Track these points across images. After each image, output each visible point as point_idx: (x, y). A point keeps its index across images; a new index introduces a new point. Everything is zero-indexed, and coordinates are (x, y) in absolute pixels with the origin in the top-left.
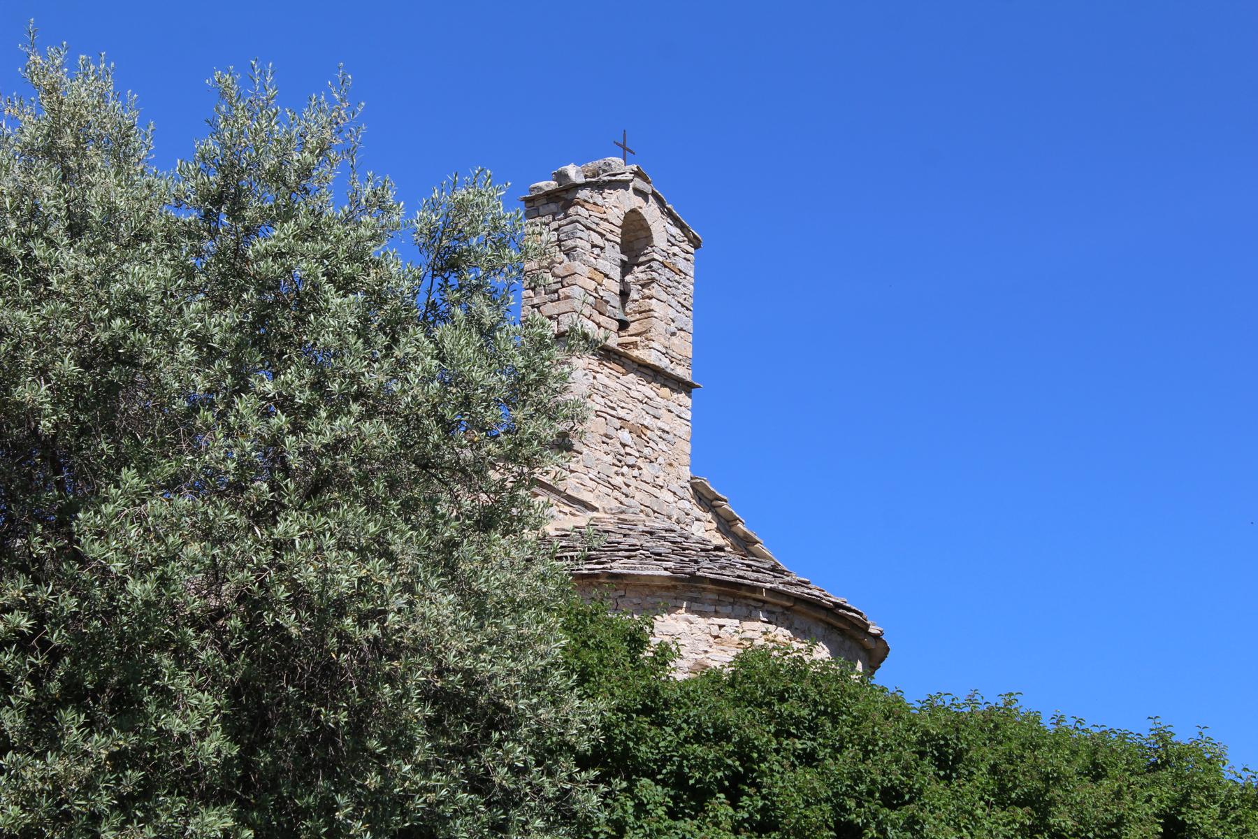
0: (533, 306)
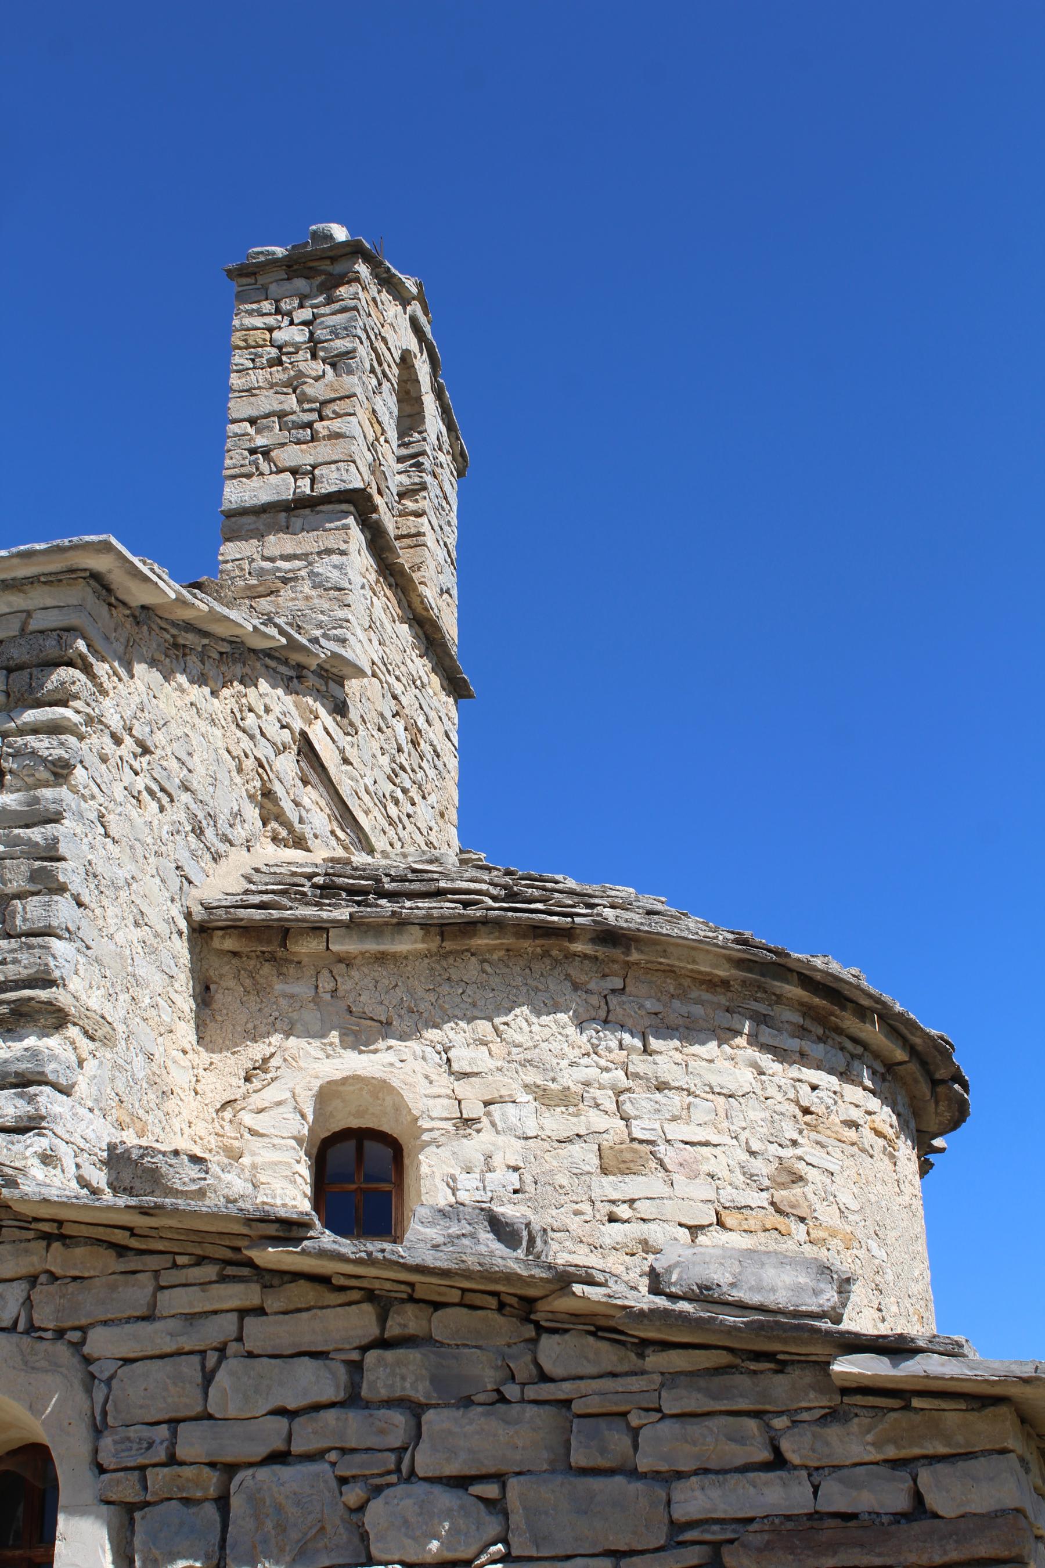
0: (253, 451)
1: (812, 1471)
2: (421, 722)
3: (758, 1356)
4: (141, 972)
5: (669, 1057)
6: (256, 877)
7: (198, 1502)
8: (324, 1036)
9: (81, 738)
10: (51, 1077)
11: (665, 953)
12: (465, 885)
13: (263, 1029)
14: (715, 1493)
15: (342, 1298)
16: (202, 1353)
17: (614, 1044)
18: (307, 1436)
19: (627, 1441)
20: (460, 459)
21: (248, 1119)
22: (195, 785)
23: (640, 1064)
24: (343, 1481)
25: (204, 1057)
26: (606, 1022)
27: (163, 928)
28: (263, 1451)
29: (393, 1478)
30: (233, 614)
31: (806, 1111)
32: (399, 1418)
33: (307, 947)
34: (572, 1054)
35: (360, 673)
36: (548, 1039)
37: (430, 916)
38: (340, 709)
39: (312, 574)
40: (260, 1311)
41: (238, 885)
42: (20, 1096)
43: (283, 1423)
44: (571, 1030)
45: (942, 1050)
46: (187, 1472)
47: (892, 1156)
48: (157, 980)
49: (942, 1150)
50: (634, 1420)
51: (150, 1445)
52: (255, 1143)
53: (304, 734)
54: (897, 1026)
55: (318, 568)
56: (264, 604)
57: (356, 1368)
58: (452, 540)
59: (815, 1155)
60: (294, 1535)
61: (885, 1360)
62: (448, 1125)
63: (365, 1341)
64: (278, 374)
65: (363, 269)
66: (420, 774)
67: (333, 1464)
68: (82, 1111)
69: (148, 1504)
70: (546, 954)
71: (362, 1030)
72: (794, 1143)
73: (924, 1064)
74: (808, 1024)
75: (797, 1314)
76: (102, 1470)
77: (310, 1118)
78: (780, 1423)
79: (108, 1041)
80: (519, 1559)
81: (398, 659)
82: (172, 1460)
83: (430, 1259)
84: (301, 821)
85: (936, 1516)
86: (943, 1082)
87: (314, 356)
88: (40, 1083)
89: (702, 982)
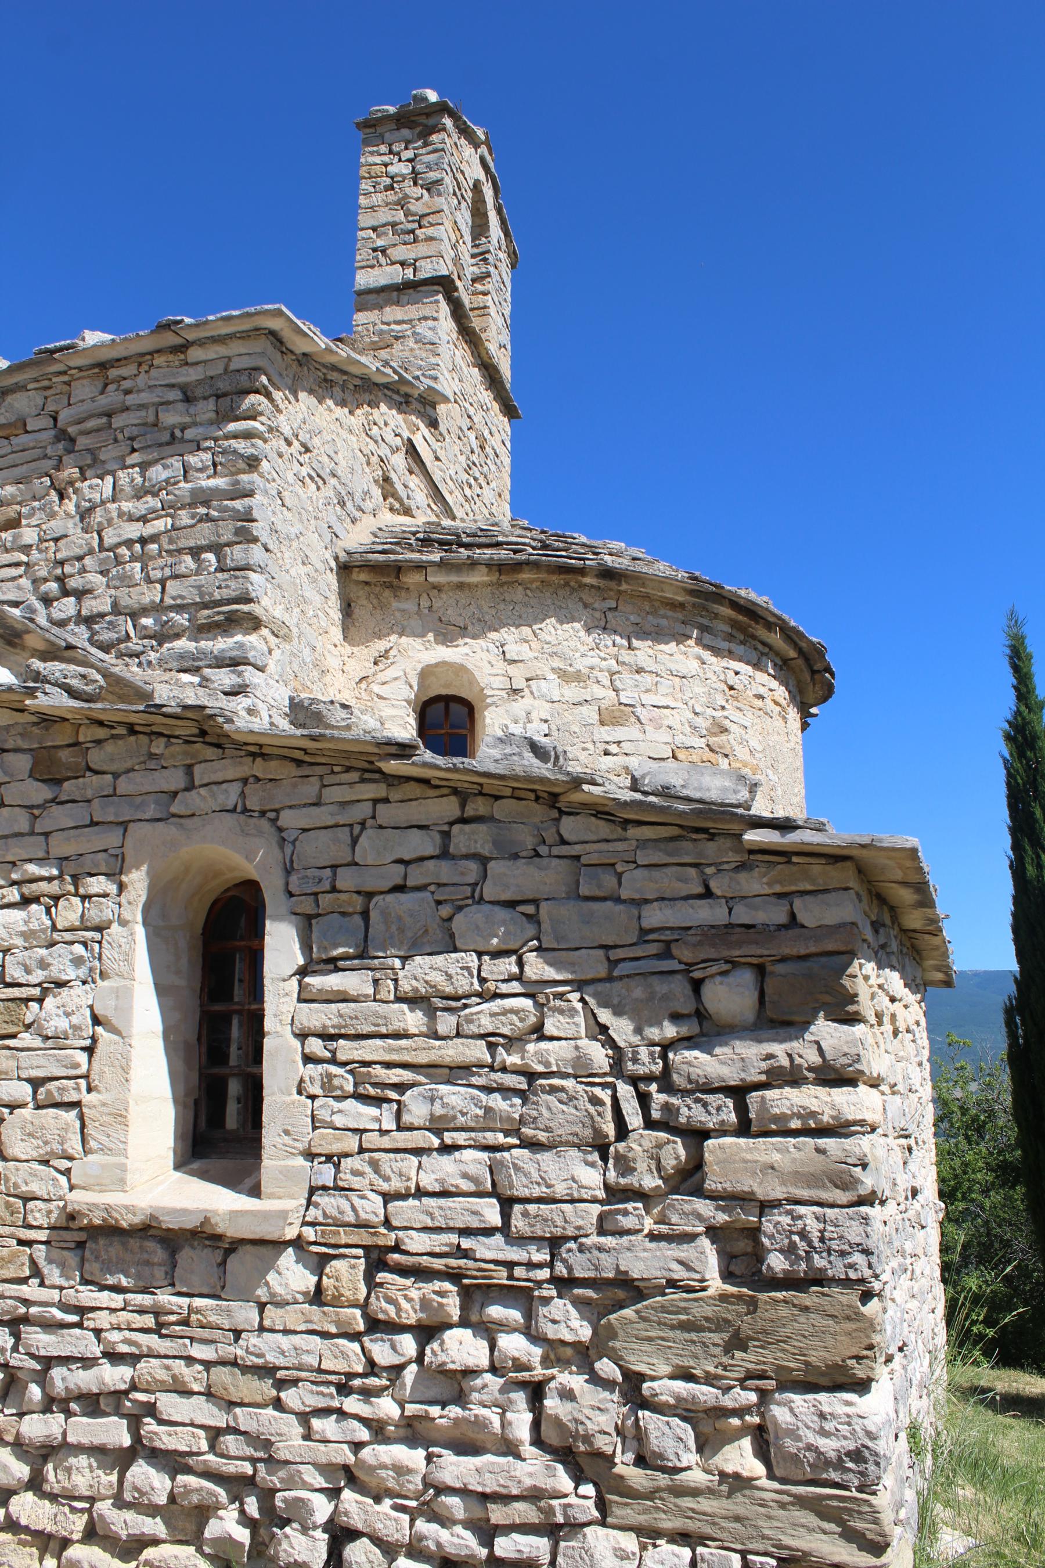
0: (375, 250)
1: (728, 899)
2: (486, 433)
3: (698, 830)
4: (307, 594)
5: (644, 651)
6: (379, 534)
7: (350, 914)
8: (424, 636)
9: (265, 441)
10: (252, 660)
11: (643, 585)
12: (515, 539)
13: (385, 631)
14: (668, 912)
15: (437, 792)
16: (351, 825)
17: (610, 643)
18: (416, 876)
19: (615, 880)
20: (513, 255)
21: (376, 688)
22: (339, 473)
23: (626, 656)
24: (439, 903)
25: (348, 649)
26: (605, 628)
27: (320, 566)
28: (390, 884)
29: (470, 901)
30: (363, 359)
31: (731, 688)
32: (473, 866)
33: (412, 579)
34: (583, 649)
35: (446, 400)
36: (568, 638)
37: (492, 559)
38: (433, 424)
39: (414, 333)
40: (386, 800)
41: (368, 539)
42: (233, 672)
43: (401, 868)
44: (582, 633)
45: (819, 651)
46: (343, 897)
47: (784, 718)
48: (317, 599)
49: (816, 715)
50: (619, 868)
51: (320, 881)
52: (382, 704)
53: (410, 440)
54: (791, 635)
55: (419, 330)
56: (383, 354)
57: (446, 835)
58: (507, 312)
59: (736, 715)
60: (410, 934)
61: (777, 832)
62: (503, 693)
63: (451, 819)
64: (391, 196)
65: (448, 122)
66: (486, 468)
67: (433, 893)
68: (272, 682)
69: (319, 915)
70: (567, 584)
71: (448, 632)
72: (723, 708)
73: (807, 659)
74: (734, 633)
75: (723, 805)
76: (291, 895)
77: (416, 688)
78: (709, 871)
79: (287, 638)
80: (547, 950)
81: (472, 392)
82: (334, 890)
83: (493, 768)
84: (408, 497)
85: (803, 926)
86: (819, 671)
87: (415, 184)
88: (245, 664)
89: (667, 604)
